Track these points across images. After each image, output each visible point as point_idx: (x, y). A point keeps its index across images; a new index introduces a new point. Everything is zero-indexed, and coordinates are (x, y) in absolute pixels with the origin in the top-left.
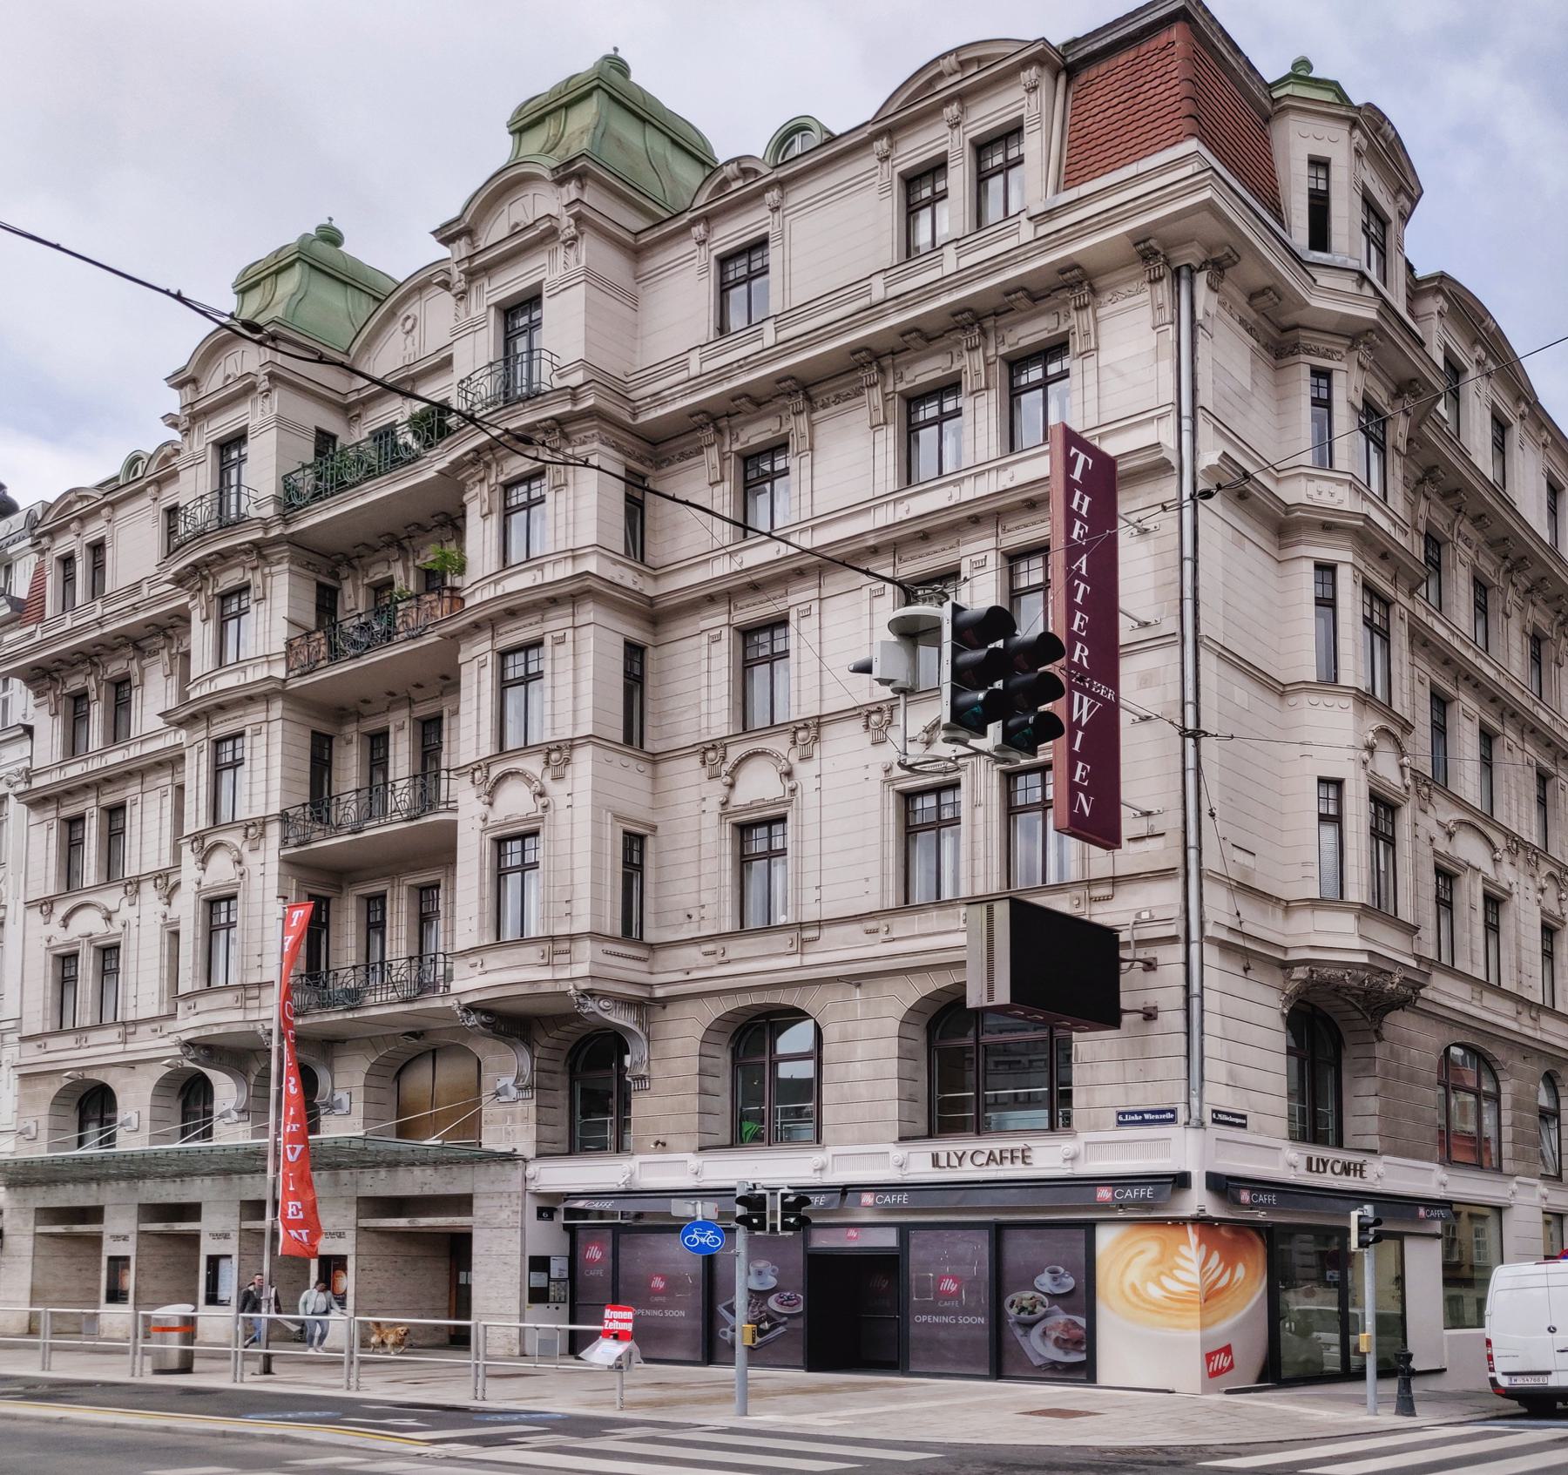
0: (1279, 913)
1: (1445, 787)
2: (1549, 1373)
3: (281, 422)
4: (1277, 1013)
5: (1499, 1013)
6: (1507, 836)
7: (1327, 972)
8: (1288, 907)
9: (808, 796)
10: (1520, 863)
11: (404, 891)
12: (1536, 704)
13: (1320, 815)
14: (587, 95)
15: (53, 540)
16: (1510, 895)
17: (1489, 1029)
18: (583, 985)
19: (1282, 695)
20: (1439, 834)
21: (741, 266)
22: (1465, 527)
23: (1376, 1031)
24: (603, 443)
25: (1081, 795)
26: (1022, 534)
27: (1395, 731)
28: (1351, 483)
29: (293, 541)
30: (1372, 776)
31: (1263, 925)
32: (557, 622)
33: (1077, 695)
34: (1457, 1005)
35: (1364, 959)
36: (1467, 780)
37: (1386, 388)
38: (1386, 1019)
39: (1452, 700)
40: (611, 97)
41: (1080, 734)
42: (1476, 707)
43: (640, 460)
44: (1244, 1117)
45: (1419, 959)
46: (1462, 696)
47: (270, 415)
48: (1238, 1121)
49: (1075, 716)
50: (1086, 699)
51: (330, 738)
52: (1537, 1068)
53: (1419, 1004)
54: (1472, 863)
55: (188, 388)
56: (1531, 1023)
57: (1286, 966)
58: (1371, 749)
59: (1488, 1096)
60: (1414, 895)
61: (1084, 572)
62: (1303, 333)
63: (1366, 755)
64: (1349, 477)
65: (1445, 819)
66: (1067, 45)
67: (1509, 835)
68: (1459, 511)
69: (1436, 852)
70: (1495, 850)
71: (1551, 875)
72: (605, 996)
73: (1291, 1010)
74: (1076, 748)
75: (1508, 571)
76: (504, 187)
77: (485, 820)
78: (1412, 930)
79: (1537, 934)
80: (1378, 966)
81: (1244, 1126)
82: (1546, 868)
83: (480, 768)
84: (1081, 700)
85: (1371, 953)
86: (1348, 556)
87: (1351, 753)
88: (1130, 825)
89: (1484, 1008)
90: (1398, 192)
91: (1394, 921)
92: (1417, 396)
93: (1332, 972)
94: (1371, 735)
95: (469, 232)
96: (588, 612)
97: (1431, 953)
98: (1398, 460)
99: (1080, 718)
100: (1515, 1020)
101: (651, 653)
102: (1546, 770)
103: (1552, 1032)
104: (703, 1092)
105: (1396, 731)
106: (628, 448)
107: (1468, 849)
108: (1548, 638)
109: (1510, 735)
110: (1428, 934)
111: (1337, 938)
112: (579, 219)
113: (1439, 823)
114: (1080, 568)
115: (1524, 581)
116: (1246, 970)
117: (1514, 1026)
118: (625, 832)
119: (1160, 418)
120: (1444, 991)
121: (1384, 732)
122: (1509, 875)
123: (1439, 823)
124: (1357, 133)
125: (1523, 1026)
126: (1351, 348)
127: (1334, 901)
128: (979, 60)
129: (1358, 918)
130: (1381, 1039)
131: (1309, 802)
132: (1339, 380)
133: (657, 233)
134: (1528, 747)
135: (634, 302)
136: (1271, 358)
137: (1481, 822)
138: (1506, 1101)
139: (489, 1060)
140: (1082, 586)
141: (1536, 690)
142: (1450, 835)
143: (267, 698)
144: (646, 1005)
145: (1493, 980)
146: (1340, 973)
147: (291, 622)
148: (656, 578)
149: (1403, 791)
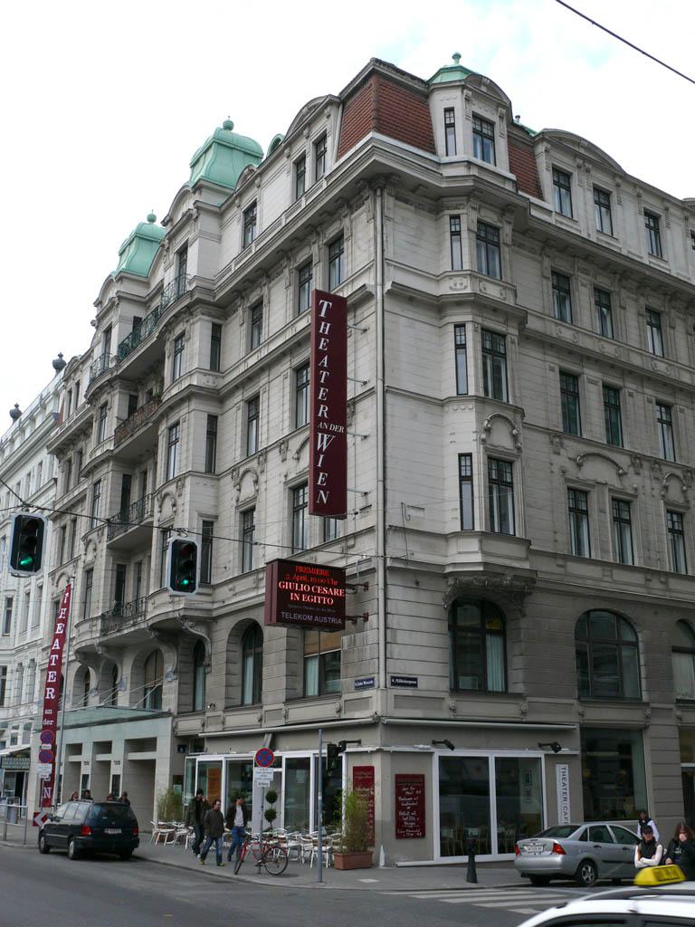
3: (122, 319)
7: (465, 579)
9: (262, 497)
11: (132, 565)
14: (210, 147)
15: (241, 201)
18: (182, 613)
19: (442, 406)
21: (249, 218)
22: (581, 264)
23: (520, 610)
24: (203, 314)
25: (322, 492)
26: (298, 359)
28: (470, 275)
29: (117, 377)
32: (184, 410)
33: (320, 435)
35: (481, 569)
37: (496, 213)
38: (525, 600)
40: (140, 238)
41: (322, 456)
43: (218, 318)
44: (416, 679)
46: (586, 371)
47: (118, 317)
49: (319, 447)
50: (325, 435)
51: (130, 476)
54: (599, 480)
55: (170, 224)
56: (661, 586)
57: (446, 576)
58: (488, 430)
61: (325, 365)
62: (444, 199)
64: (469, 272)
66: (341, 94)
69: (567, 480)
72: (191, 618)
76: (182, 196)
77: (286, 476)
83: (283, 443)
84: (323, 437)
86: (469, 318)
88: (353, 502)
90: (498, 107)
92: (512, 212)
93: (466, 578)
95: (171, 220)
96: (194, 404)
98: (507, 249)
99: (322, 447)
101: (220, 419)
103: (680, 591)
104: (228, 673)
106: (213, 313)
107: (596, 471)
109: (630, 386)
111: (467, 555)
112: (198, 208)
113: (570, 459)
114: (323, 364)
116: (417, 583)
118: (204, 521)
119: (369, 268)
122: (633, 481)
124: (465, 91)
126: (468, 201)
127: (465, 533)
128: (314, 106)
129: (481, 542)
130: (524, 616)
132: (463, 218)
133: (231, 200)
135: (219, 239)
136: (434, 216)
139: (166, 656)
140: (325, 373)
143: (103, 462)
144: (209, 621)
147: (117, 417)
148: (223, 377)
149: (515, 452)
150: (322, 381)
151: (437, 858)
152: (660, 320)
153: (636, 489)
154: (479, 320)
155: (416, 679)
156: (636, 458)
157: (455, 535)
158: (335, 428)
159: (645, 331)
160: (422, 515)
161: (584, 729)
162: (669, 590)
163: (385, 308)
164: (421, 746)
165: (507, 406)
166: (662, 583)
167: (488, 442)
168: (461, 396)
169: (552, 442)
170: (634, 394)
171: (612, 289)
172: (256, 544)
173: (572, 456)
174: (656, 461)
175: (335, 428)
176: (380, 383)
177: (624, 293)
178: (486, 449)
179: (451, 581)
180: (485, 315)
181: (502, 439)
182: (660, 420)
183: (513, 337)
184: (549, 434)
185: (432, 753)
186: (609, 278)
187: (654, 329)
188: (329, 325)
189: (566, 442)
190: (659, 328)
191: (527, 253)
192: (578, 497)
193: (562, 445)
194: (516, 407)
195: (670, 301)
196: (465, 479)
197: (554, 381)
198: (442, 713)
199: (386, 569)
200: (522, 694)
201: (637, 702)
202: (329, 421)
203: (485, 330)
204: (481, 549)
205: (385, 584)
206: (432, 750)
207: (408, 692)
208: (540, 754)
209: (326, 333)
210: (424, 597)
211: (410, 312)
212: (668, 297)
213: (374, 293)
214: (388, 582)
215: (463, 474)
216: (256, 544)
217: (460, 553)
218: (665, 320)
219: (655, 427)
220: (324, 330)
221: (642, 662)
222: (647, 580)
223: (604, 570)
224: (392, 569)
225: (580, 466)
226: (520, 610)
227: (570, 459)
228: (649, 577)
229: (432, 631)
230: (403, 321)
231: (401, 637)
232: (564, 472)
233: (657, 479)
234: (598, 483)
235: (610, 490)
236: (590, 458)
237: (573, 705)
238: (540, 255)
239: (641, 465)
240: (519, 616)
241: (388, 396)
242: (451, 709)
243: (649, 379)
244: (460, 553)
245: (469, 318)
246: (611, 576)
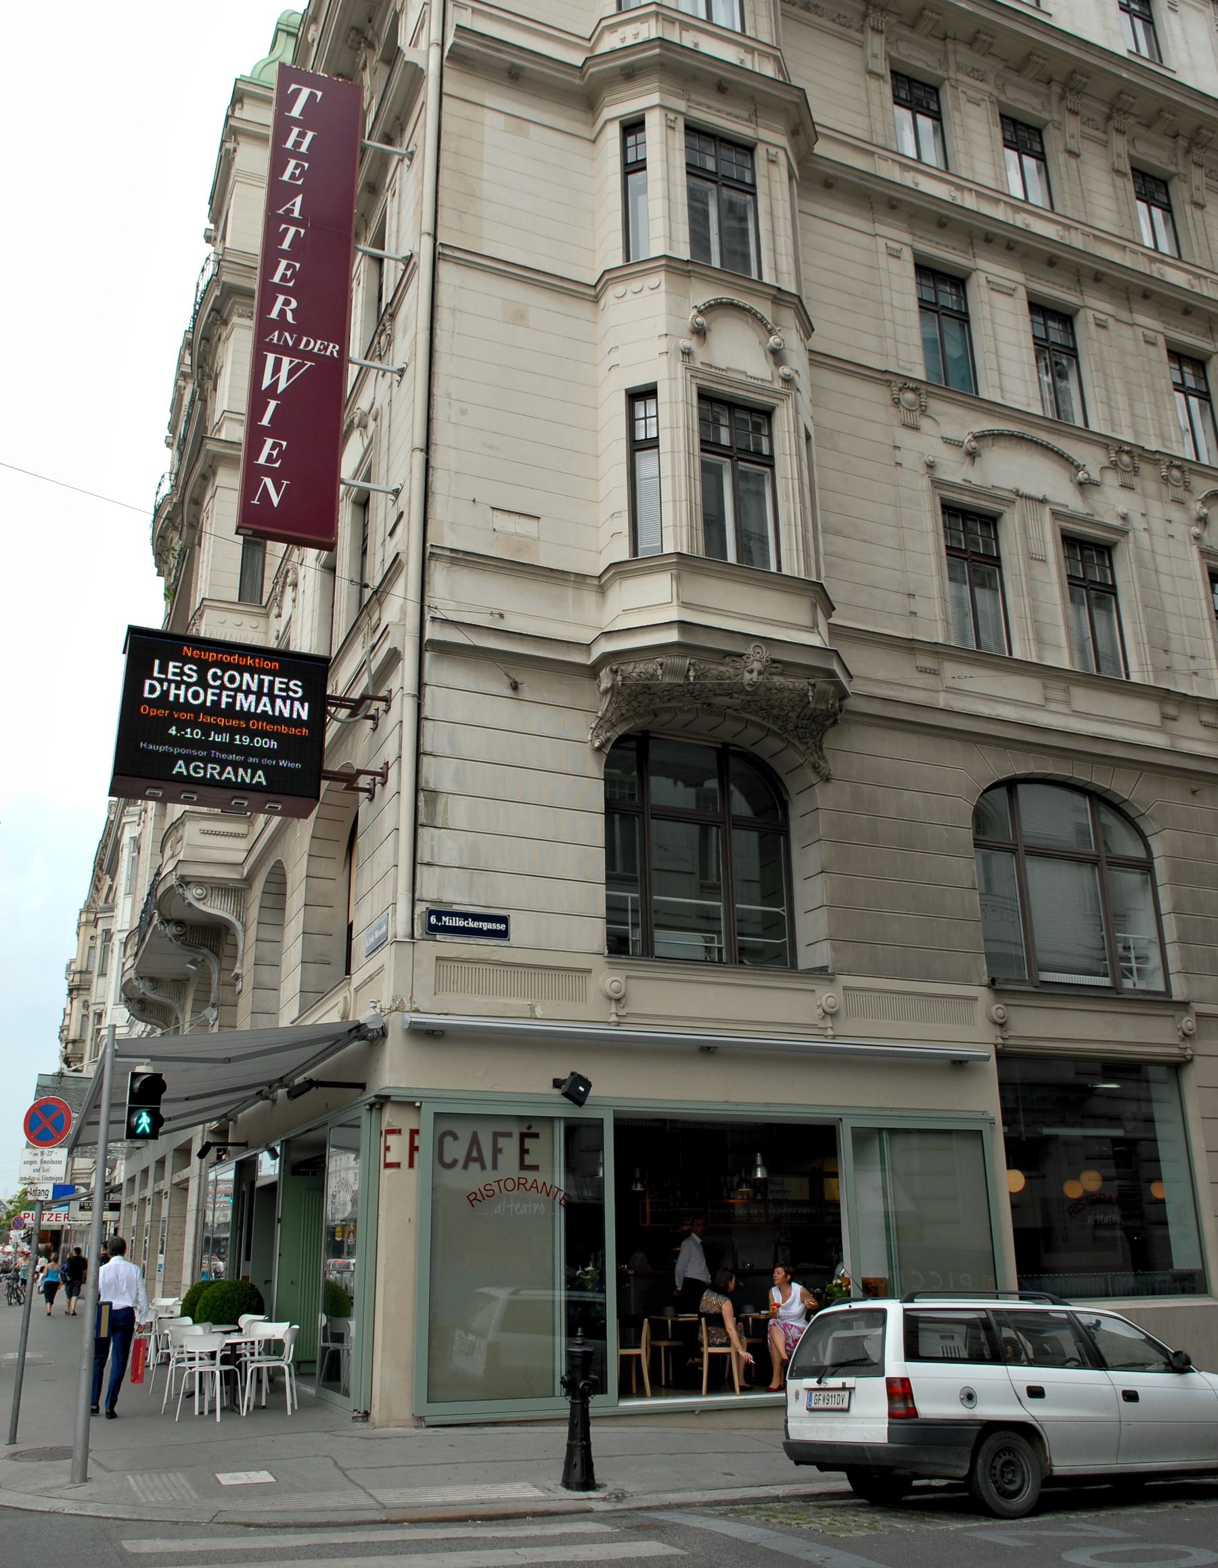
0: (590, 598)
7: (635, 669)
10: (1151, 486)
22: (964, 55)
25: (268, 481)
28: (657, 14)
31: (530, 613)
33: (271, 358)
34: (1010, 713)
35: (672, 636)
39: (969, 273)
41: (273, 404)
44: (504, 920)
46: (982, 264)
49: (267, 382)
50: (286, 361)
54: (1026, 489)
58: (700, 332)
61: (296, 214)
64: (653, 8)
65: (954, 433)
67: (1104, 442)
68: (944, 39)
69: (937, 483)
72: (200, 882)
74: (265, 421)
81: (504, 934)
85: (683, 625)
87: (663, 345)
89: (1077, 714)
93: (641, 667)
99: (275, 384)
107: (1009, 471)
108: (1174, 175)
109: (1094, 307)
111: (648, 608)
113: (947, 441)
116: (515, 687)
122: (1113, 503)
123: (947, 441)
127: (637, 563)
129: (678, 579)
130: (827, 779)
138: (1159, 865)
149: (778, 385)
150: (285, 245)
152: (1205, 378)
153: (1124, 518)
154: (681, 105)
155: (504, 920)
156: (1120, 451)
158: (316, 346)
159: (1134, 218)
160: (534, 534)
161: (1003, 1056)
163: (445, 90)
165: (759, 288)
167: (700, 356)
168: (632, 265)
169: (897, 402)
170: (1111, 322)
171: (1045, 116)
174: (1176, 463)
175: (316, 346)
176: (427, 242)
177: (1073, 125)
178: (693, 372)
180: (693, 96)
181: (739, 355)
182: (1180, 387)
183: (773, 150)
184: (888, 383)
186: (1037, 94)
187: (1194, 401)
188: (310, 135)
189: (935, 406)
190: (1167, 209)
191: (824, 22)
192: (971, 535)
193: (924, 411)
194: (779, 289)
195: (1188, 151)
197: (904, 288)
199: (423, 646)
201: (1163, 1002)
202: (299, 330)
203: (693, 130)
205: (421, 685)
209: (304, 149)
210: (536, 718)
211: (498, 99)
212: (1182, 143)
213: (421, 65)
215: (640, 436)
218: (1179, 193)
219: (1173, 401)
220: (297, 144)
222: (1165, 717)
223: (1045, 687)
224: (445, 649)
225: (972, 455)
226: (815, 768)
228: (1171, 710)
230: (491, 120)
231: (457, 811)
232: (931, 466)
233: (1180, 502)
234: (1021, 496)
235: (1055, 514)
236: (1003, 443)
237: (975, 999)
238: (861, 30)
239: (1136, 471)
240: (813, 778)
241: (444, 269)
242: (610, 999)
243: (1146, 295)
245: (655, 99)
246: (1067, 702)
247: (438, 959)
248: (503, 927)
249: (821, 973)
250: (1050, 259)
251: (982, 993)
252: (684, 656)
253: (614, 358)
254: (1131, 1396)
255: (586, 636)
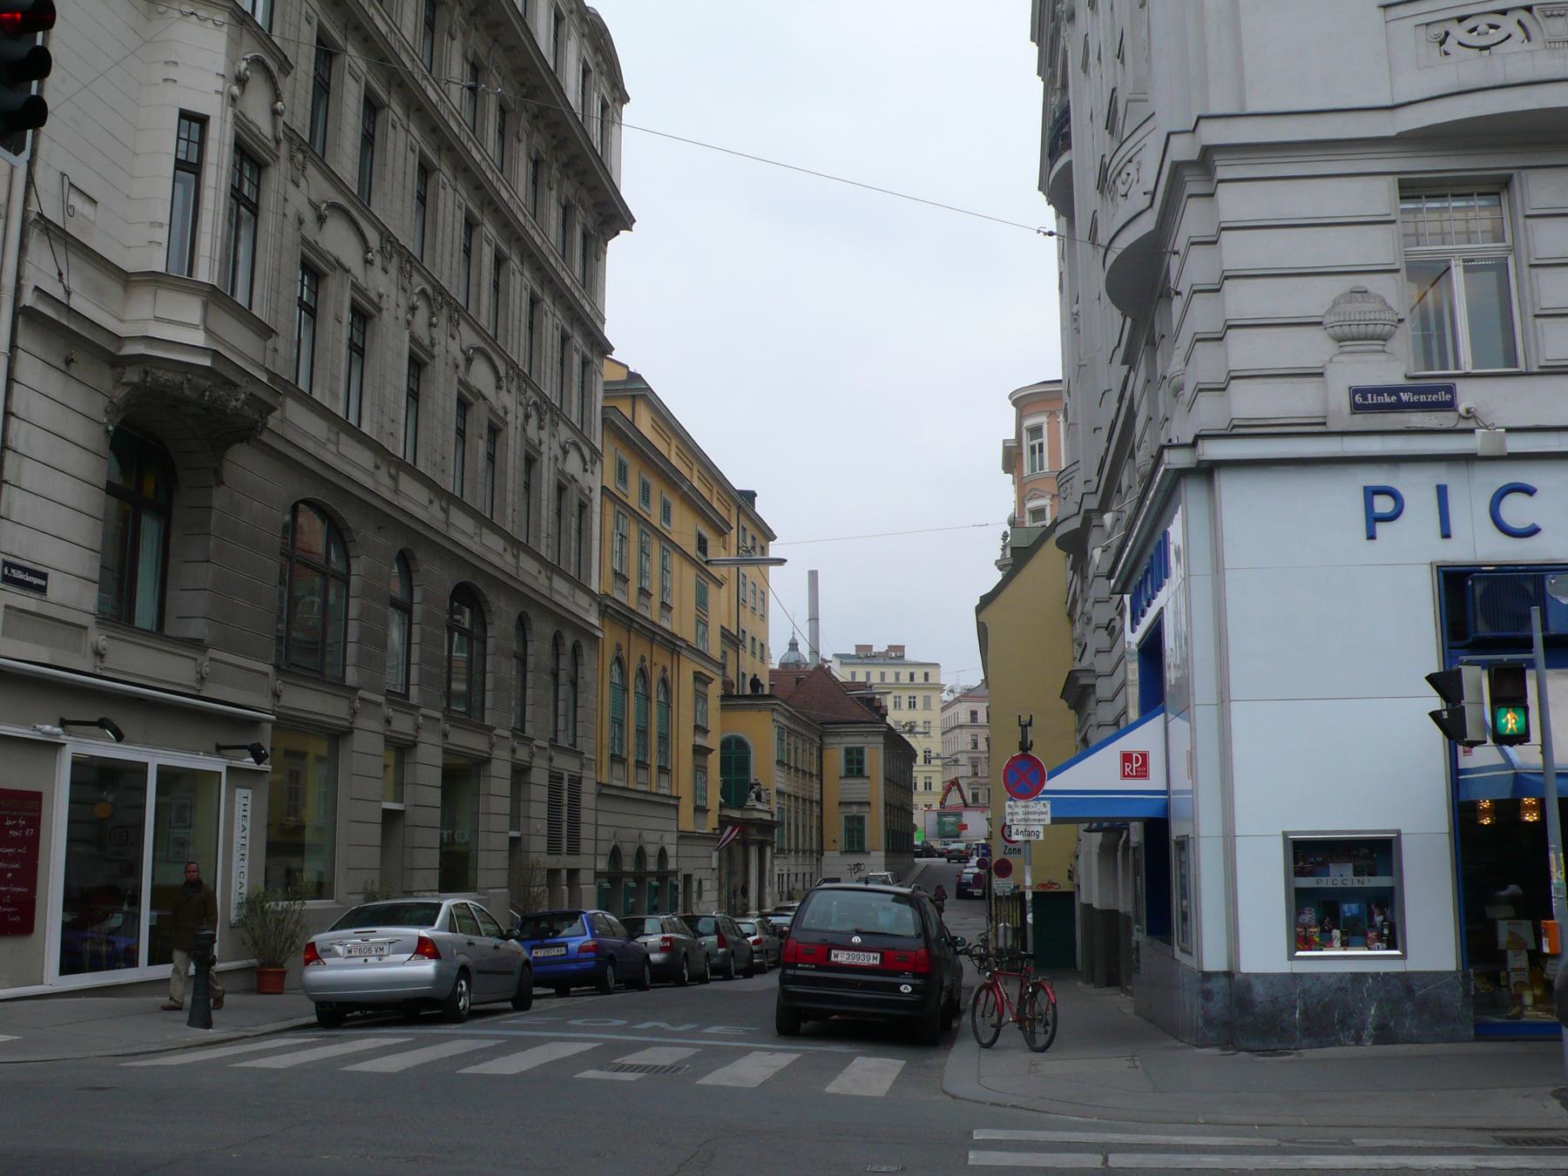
1: (322, 159)
2: (165, 1008)
4: (102, 429)
5: (355, 462)
6: (381, 234)
7: (165, 376)
8: (128, 280)
10: (393, 271)
12: (425, 77)
13: (177, 160)
16: (380, 310)
17: (403, 519)
20: (309, 216)
27: (269, 65)
30: (240, 122)
34: (310, 446)
35: (207, 362)
36: (394, 204)
42: (363, 66)
44: (44, 576)
45: (273, 376)
48: (36, 581)
52: (391, 544)
53: (265, 437)
57: (118, 363)
58: (241, 81)
59: (335, 575)
60: (272, 290)
63: (236, 90)
67: (387, 236)
70: (367, 249)
71: (423, 291)
73: (117, 429)
75: (555, 148)
78: (265, 331)
79: (452, 405)
80: (221, 373)
82: (419, 283)
85: (216, 355)
87: (219, 84)
91: (245, 315)
93: (169, 376)
94: (244, 65)
97: (288, 376)
100: (371, 475)
102: (377, 96)
105: (274, 67)
107: (338, 241)
110: (282, 344)
111: (176, 327)
115: (564, 158)
116: (69, 362)
117: (369, 484)
120: (298, 424)
121: (257, 62)
122: (382, 283)
125: (379, 482)
127: (177, 280)
129: (205, 306)
131: (165, 144)
134: (413, 129)
137: (354, 205)
138: (417, 610)
141: (426, 61)
142: (321, 219)
145: (409, 460)
146: (178, 378)
149: (272, 145)
151: (53, 980)
155: (44, 576)
157: (153, 279)
162: (397, 491)
164: (48, 728)
166: (391, 476)
172: (1051, 234)
173: (314, 198)
179: (132, 375)
185: (59, 746)
196: (189, 167)
198: (75, 661)
200: (202, 641)
201: (339, 686)
204: (205, 320)
206: (63, 738)
207: (28, 601)
208: (217, 765)
214: (20, 342)
216: (1051, 234)
217: (157, 319)
221: (353, 613)
227: (310, 202)
229: (82, 476)
233: (405, 290)
237: (266, 674)
244: (157, 319)
246: (337, 444)
247: (7, 607)
248: (42, 583)
249: (197, 645)
250: (399, 81)
251: (269, 669)
252: (207, 379)
253: (172, 72)
254: (470, 944)
255: (122, 330)
